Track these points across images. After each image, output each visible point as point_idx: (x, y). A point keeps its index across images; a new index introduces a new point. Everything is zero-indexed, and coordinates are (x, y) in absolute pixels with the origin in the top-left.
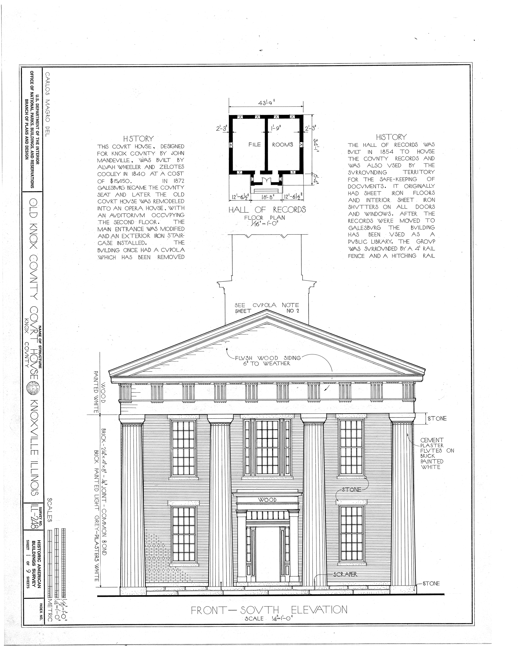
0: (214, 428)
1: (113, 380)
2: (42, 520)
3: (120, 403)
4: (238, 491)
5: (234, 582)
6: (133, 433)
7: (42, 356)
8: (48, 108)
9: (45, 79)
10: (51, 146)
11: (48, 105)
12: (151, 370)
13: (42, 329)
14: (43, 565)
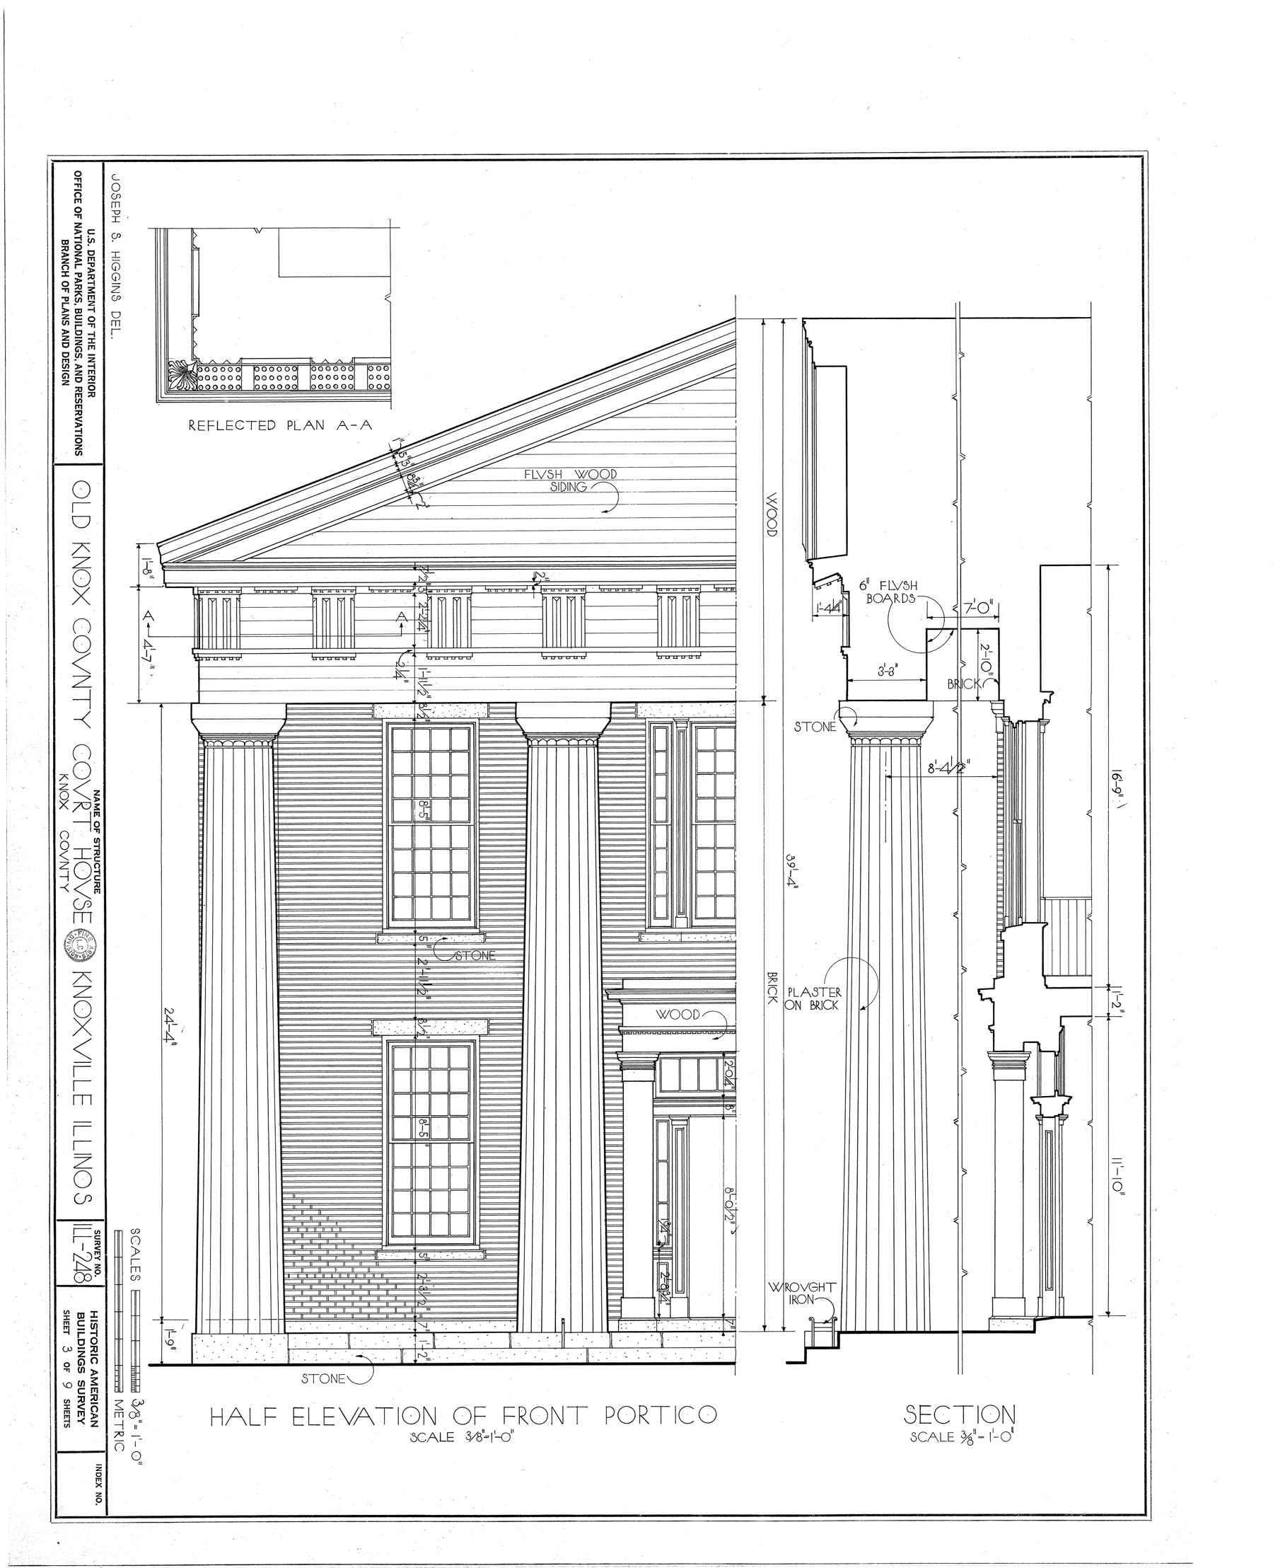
0: (540, 755)
1: (172, 576)
2: (102, 1262)
3: (198, 659)
4: (628, 984)
5: (612, 1317)
6: (242, 773)
12: (318, 538)
13: (101, 797)
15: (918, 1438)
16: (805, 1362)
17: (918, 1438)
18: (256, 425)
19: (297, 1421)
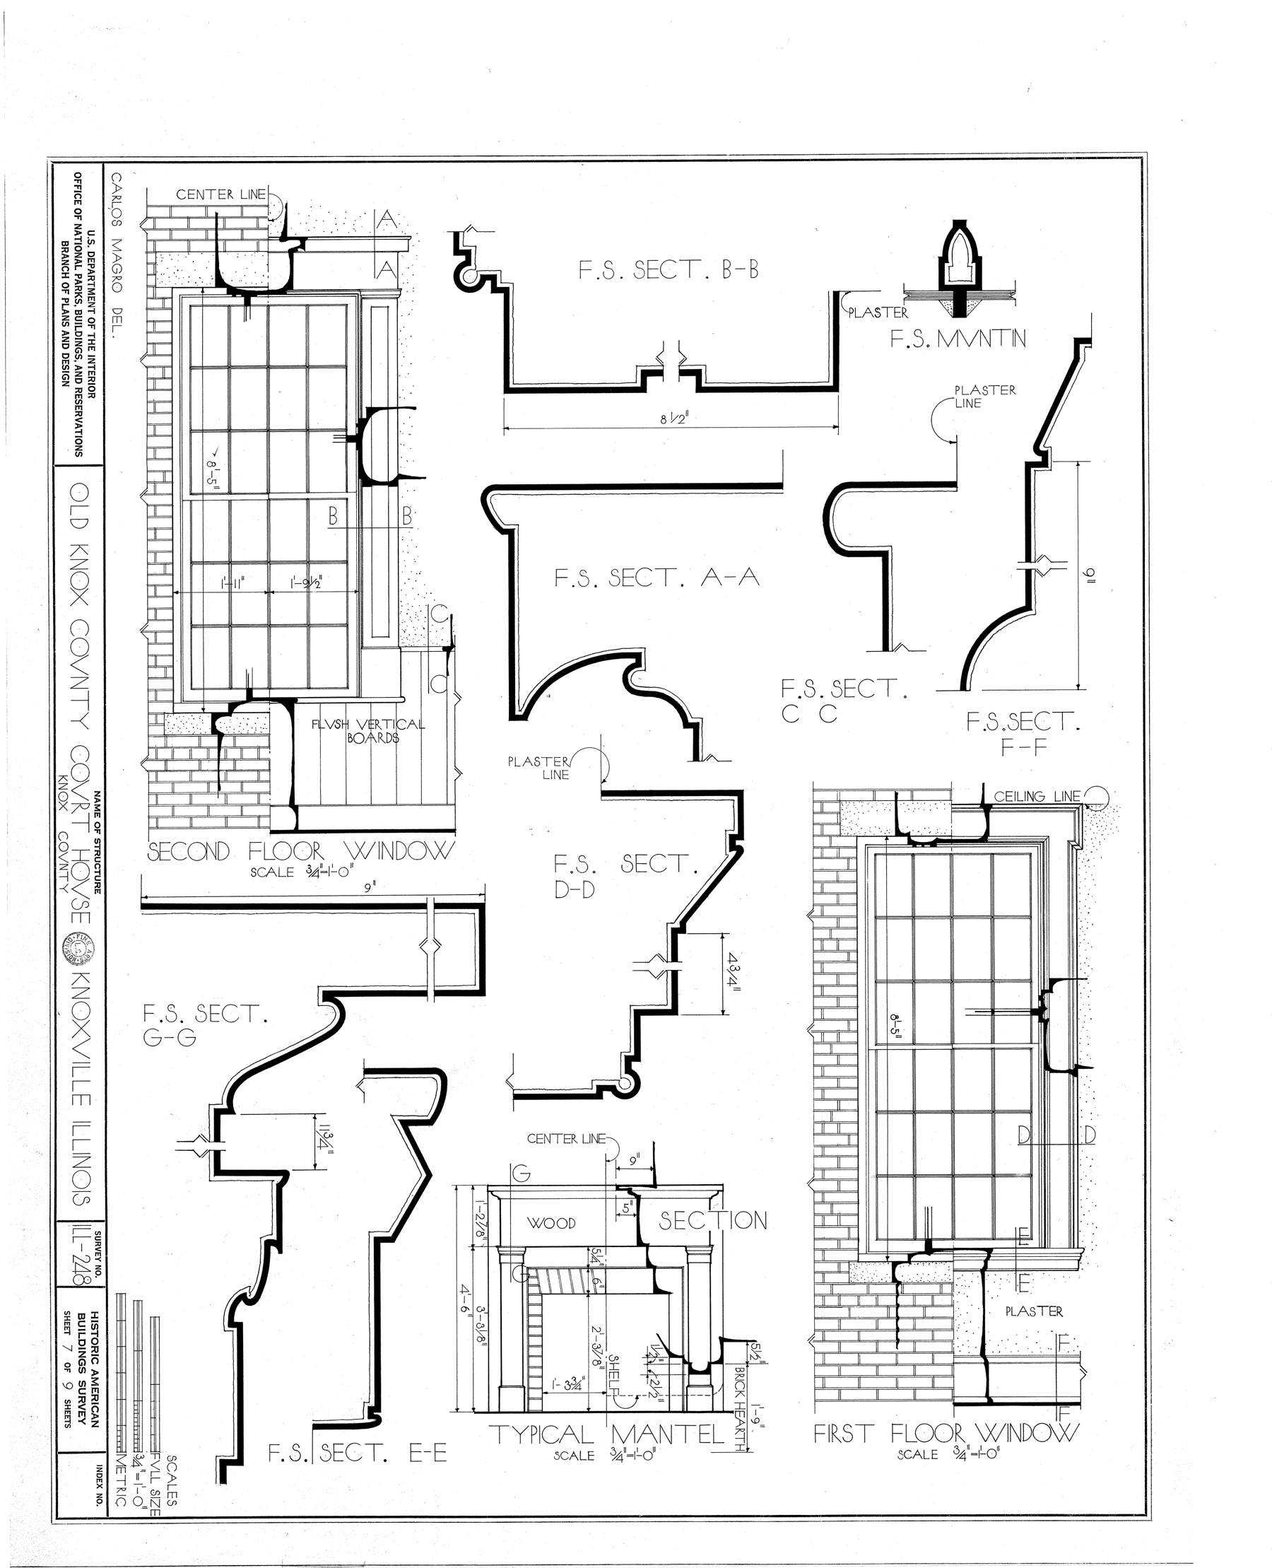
2: (103, 1264)
7: (102, 864)
8: (118, 258)
13: (102, 798)
15: (171, 1462)
16: (481, 992)
17: (171, 1462)
18: (998, 389)
19: (704, 1438)
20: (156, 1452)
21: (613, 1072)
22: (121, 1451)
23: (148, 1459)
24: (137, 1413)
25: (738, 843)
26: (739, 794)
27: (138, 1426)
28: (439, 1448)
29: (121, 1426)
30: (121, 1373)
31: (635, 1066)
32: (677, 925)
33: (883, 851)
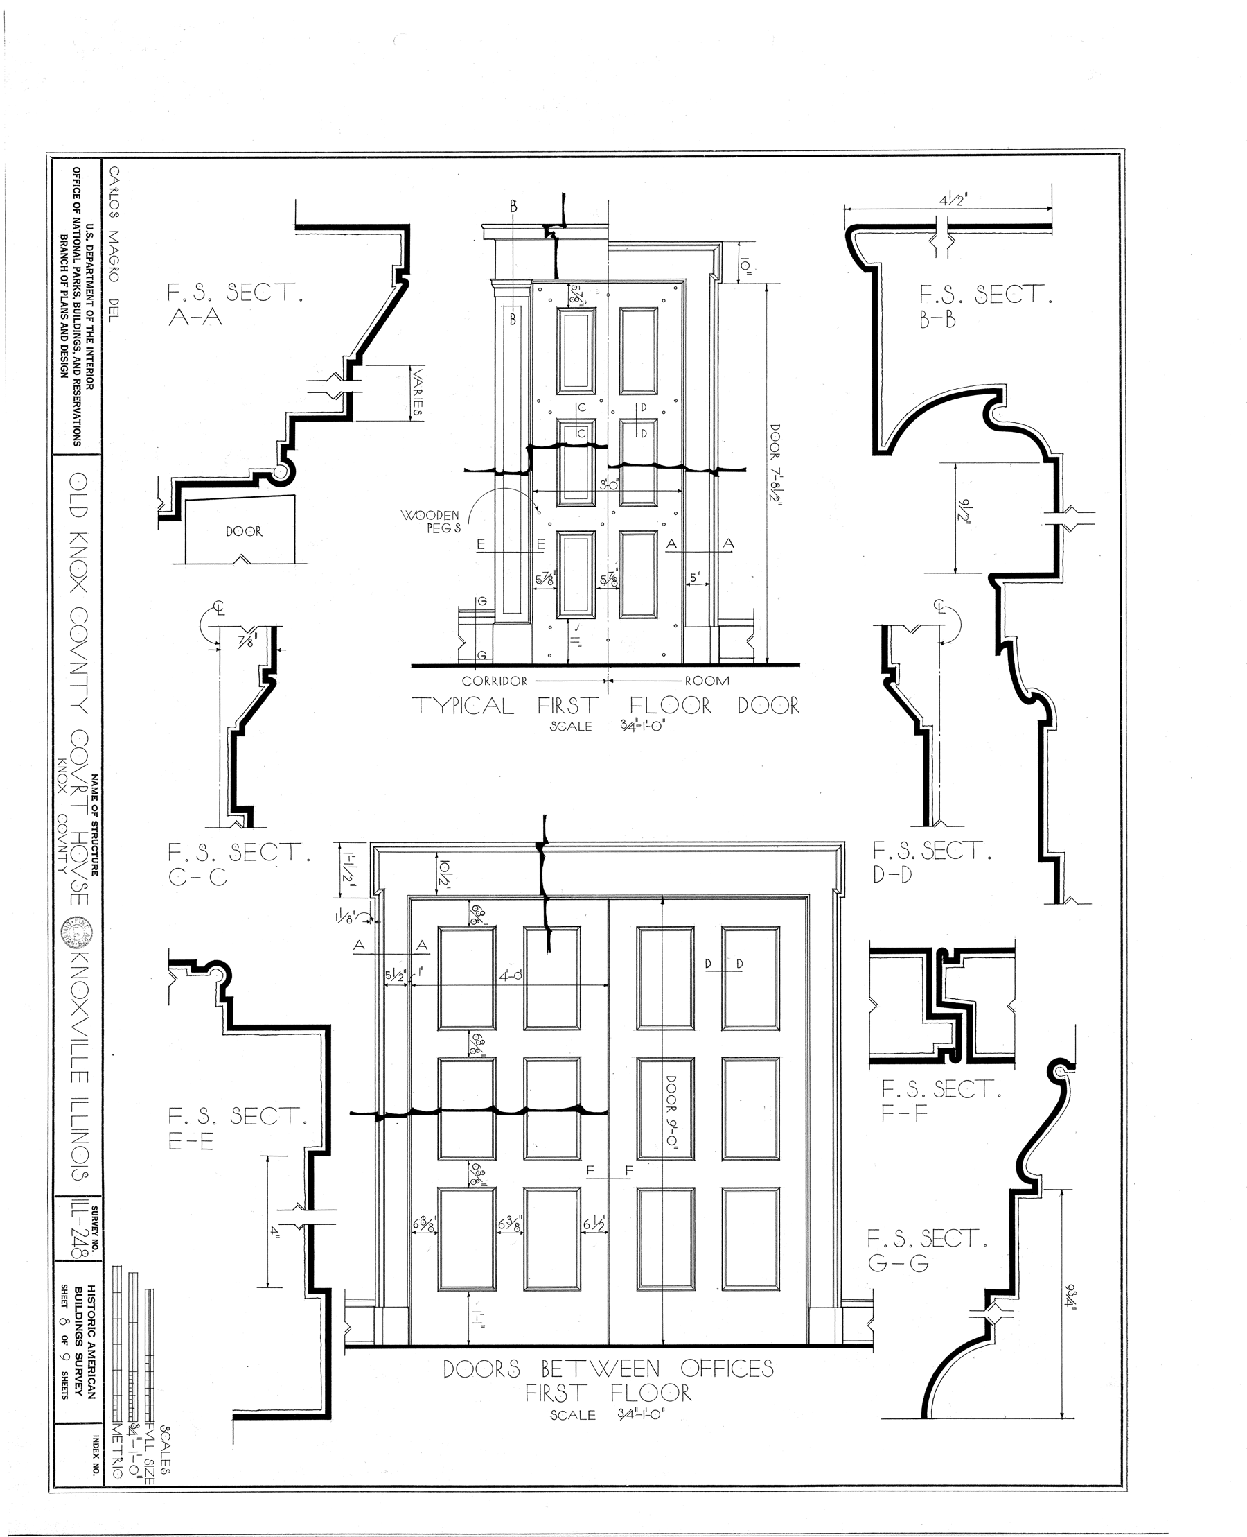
2: (100, 1238)
7: (99, 846)
8: (115, 250)
9: (108, 180)
10: (123, 346)
11: (115, 245)
13: (99, 781)
14: (99, 1344)
20: (151, 1422)
21: (269, 460)
22: (117, 1422)
23: (143, 1430)
24: (132, 1382)
25: (404, 276)
26: (406, 228)
27: (132, 1395)
28: (206, 1137)
29: (117, 1396)
30: (117, 1344)
31: (290, 454)
32: (354, 357)
33: (507, 234)
